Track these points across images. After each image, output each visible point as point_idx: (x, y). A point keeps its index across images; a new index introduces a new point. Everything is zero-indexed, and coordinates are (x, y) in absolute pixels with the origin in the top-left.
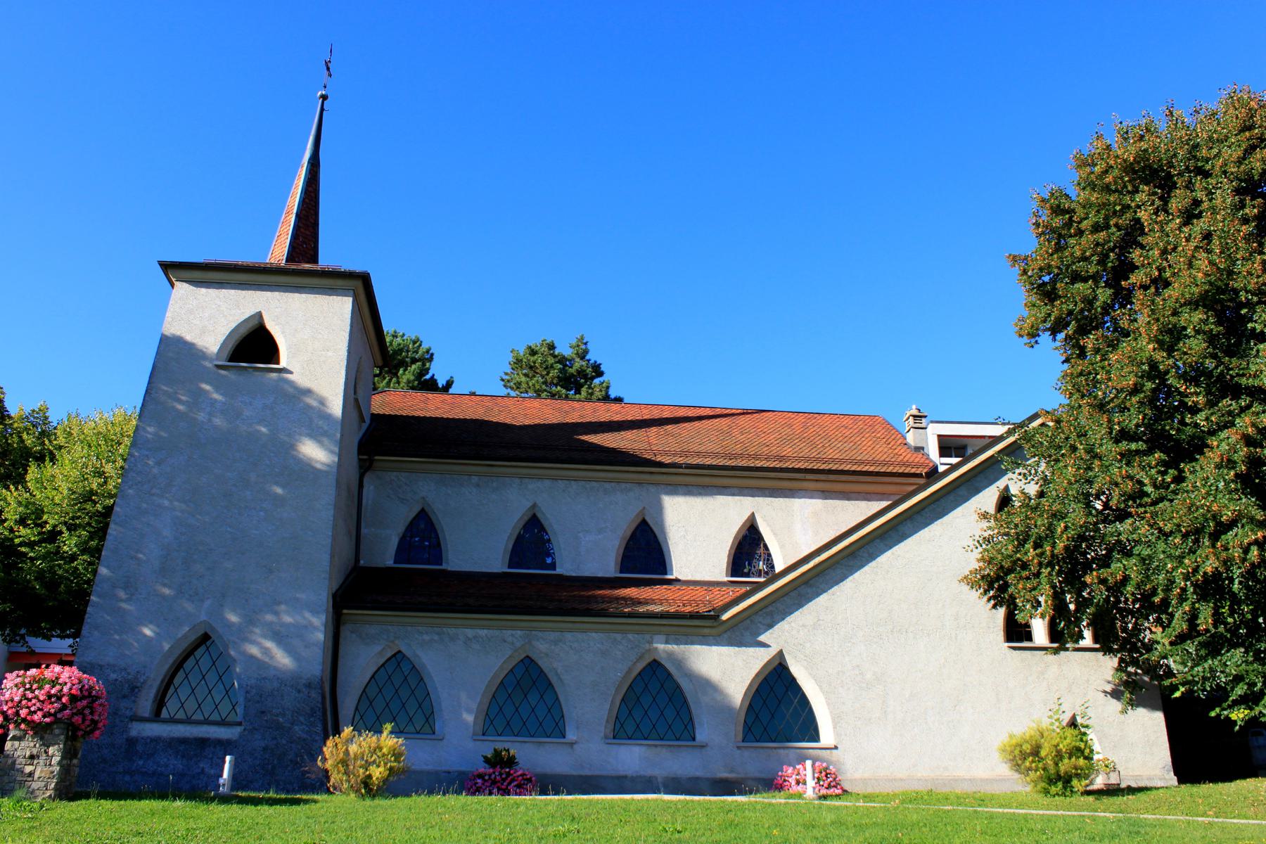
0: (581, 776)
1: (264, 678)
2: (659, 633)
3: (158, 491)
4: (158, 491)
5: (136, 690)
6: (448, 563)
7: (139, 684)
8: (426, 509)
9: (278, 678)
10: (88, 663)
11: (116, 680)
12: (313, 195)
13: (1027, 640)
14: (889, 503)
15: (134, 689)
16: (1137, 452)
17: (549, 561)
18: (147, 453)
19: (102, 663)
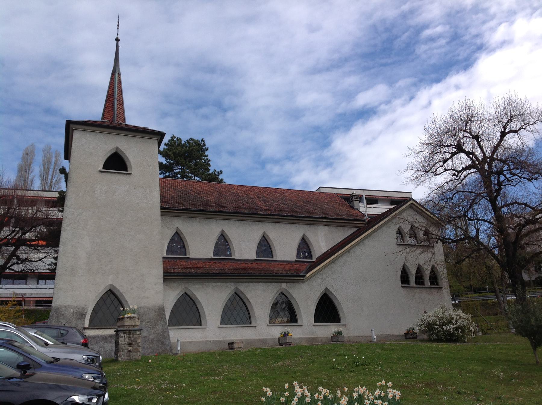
0: (259, 339)
1: (140, 307)
2: (284, 282)
3: (81, 228)
4: (81, 228)
5: (84, 316)
6: (235, 255)
7: (84, 313)
8: (178, 232)
9: (146, 307)
10: (59, 305)
11: (74, 312)
12: (120, 89)
13: (422, 284)
14: (355, 229)
15: (82, 315)
16: (42, 246)
17: (228, 253)
18: (73, 210)
19: (66, 305)
